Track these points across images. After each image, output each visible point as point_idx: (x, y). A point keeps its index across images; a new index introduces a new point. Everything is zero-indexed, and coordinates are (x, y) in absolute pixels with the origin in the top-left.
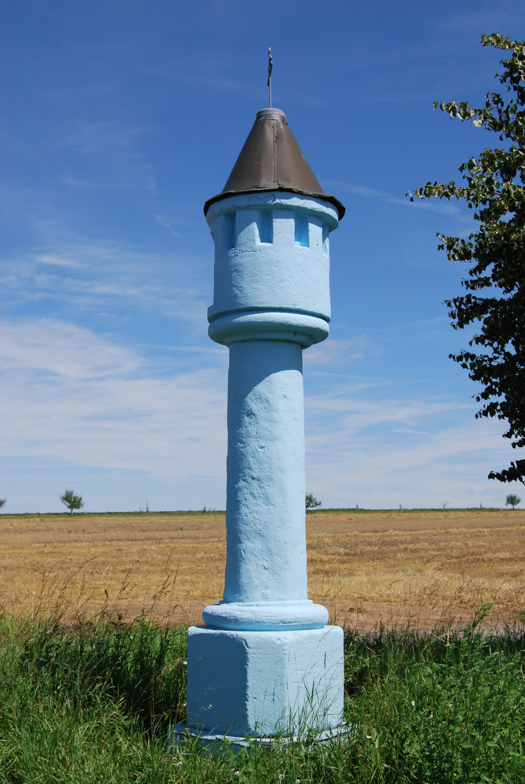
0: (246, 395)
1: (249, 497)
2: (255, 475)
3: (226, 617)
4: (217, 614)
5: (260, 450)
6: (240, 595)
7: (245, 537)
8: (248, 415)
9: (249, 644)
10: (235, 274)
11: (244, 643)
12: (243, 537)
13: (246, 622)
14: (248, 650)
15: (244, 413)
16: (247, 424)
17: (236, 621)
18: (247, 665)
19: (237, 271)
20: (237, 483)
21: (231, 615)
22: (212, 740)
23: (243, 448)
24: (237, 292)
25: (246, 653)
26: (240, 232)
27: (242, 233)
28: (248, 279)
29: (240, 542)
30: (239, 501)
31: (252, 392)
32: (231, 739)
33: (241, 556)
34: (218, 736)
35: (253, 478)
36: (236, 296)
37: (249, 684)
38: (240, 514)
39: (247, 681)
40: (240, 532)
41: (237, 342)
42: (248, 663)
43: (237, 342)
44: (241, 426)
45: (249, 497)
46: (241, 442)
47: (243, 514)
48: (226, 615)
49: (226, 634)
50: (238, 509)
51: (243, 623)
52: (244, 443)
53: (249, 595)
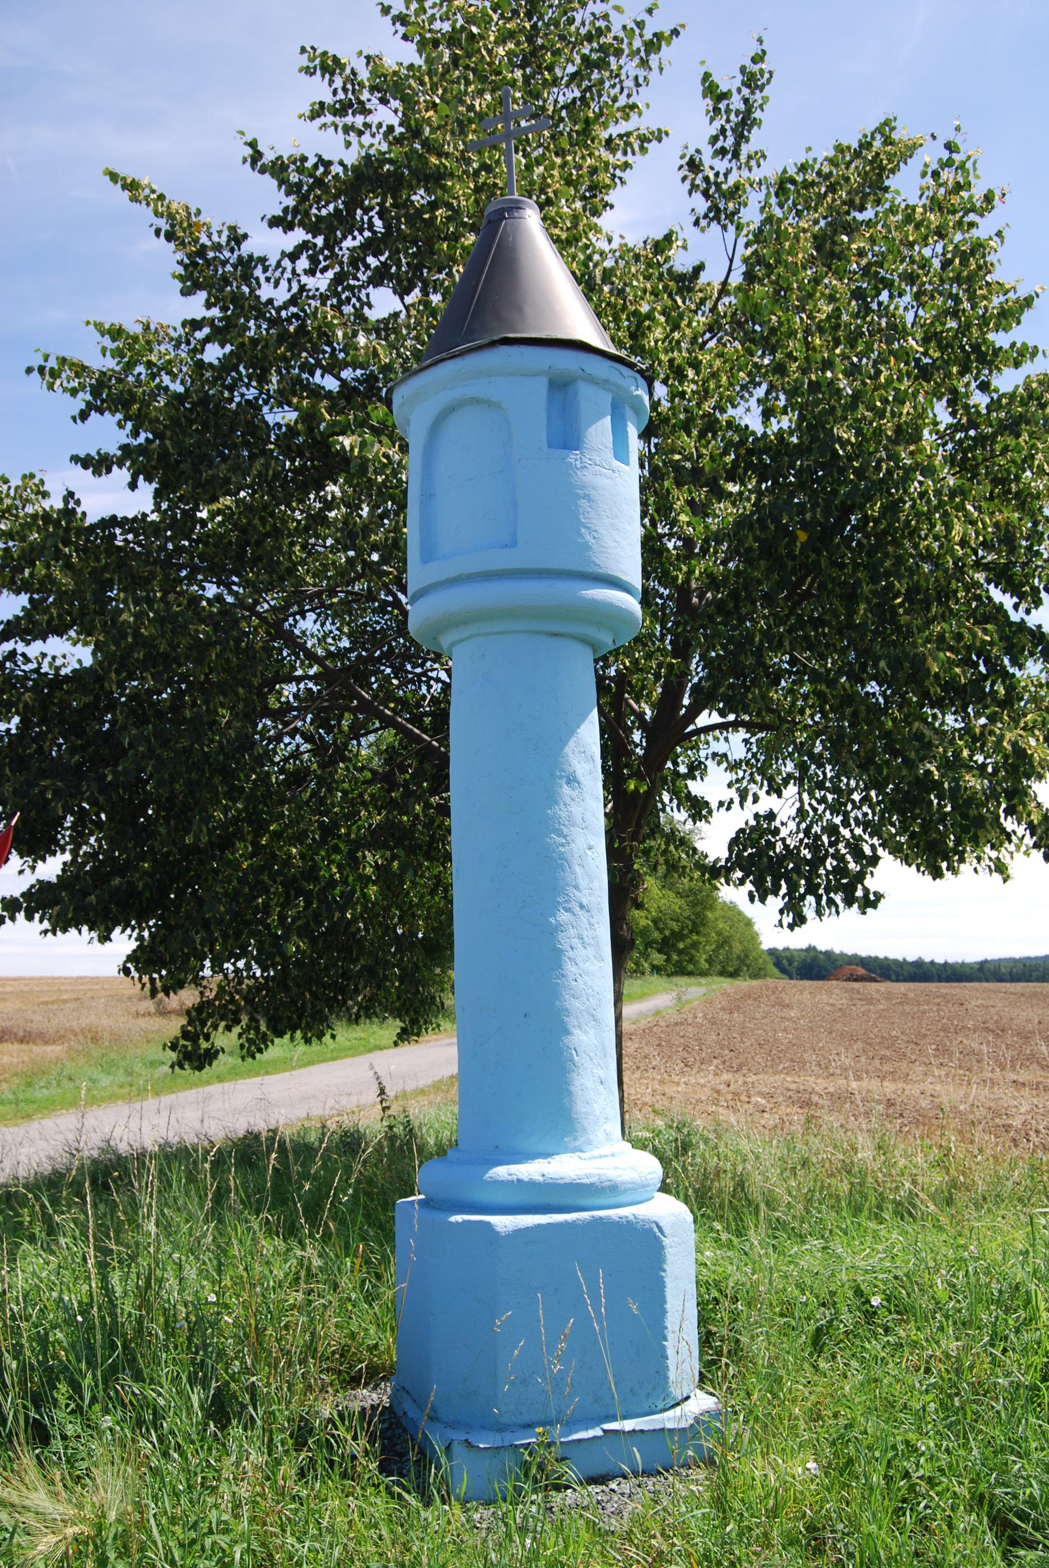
0: (564, 742)
1: (575, 942)
2: (585, 902)
3: (592, 1184)
4: (567, 1181)
5: (589, 853)
6: (575, 1139)
7: (575, 1023)
8: (568, 783)
9: (666, 1230)
10: (583, 502)
11: (656, 1229)
12: (571, 1022)
13: (631, 1189)
14: (666, 1241)
15: (561, 777)
16: (568, 800)
17: (613, 1188)
18: (664, 1271)
19: (587, 496)
20: (554, 915)
21: (603, 1178)
22: (595, 1438)
23: (563, 845)
24: (589, 538)
25: (663, 1248)
26: (589, 426)
27: (593, 427)
28: (607, 521)
29: (567, 1032)
30: (562, 951)
31: (573, 739)
32: (629, 1425)
33: (572, 1060)
34: (607, 1426)
35: (582, 906)
36: (587, 547)
37: (668, 1306)
38: (564, 976)
39: (665, 1302)
40: (567, 1012)
41: (538, 633)
42: (665, 1267)
43: (538, 633)
44: (556, 802)
45: (575, 942)
46: (560, 833)
47: (571, 977)
48: (592, 1180)
49: (608, 1218)
50: (560, 967)
51: (626, 1191)
52: (565, 837)
53: (592, 1137)
